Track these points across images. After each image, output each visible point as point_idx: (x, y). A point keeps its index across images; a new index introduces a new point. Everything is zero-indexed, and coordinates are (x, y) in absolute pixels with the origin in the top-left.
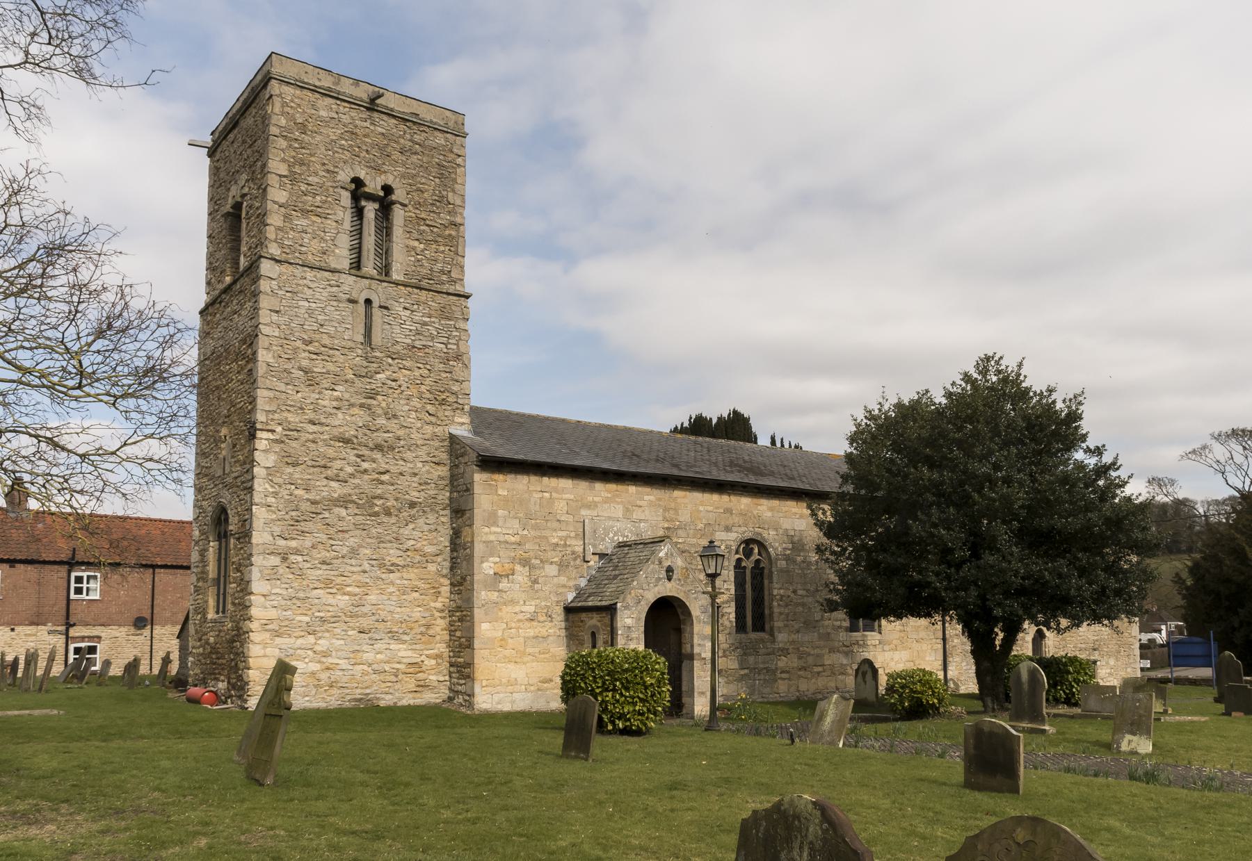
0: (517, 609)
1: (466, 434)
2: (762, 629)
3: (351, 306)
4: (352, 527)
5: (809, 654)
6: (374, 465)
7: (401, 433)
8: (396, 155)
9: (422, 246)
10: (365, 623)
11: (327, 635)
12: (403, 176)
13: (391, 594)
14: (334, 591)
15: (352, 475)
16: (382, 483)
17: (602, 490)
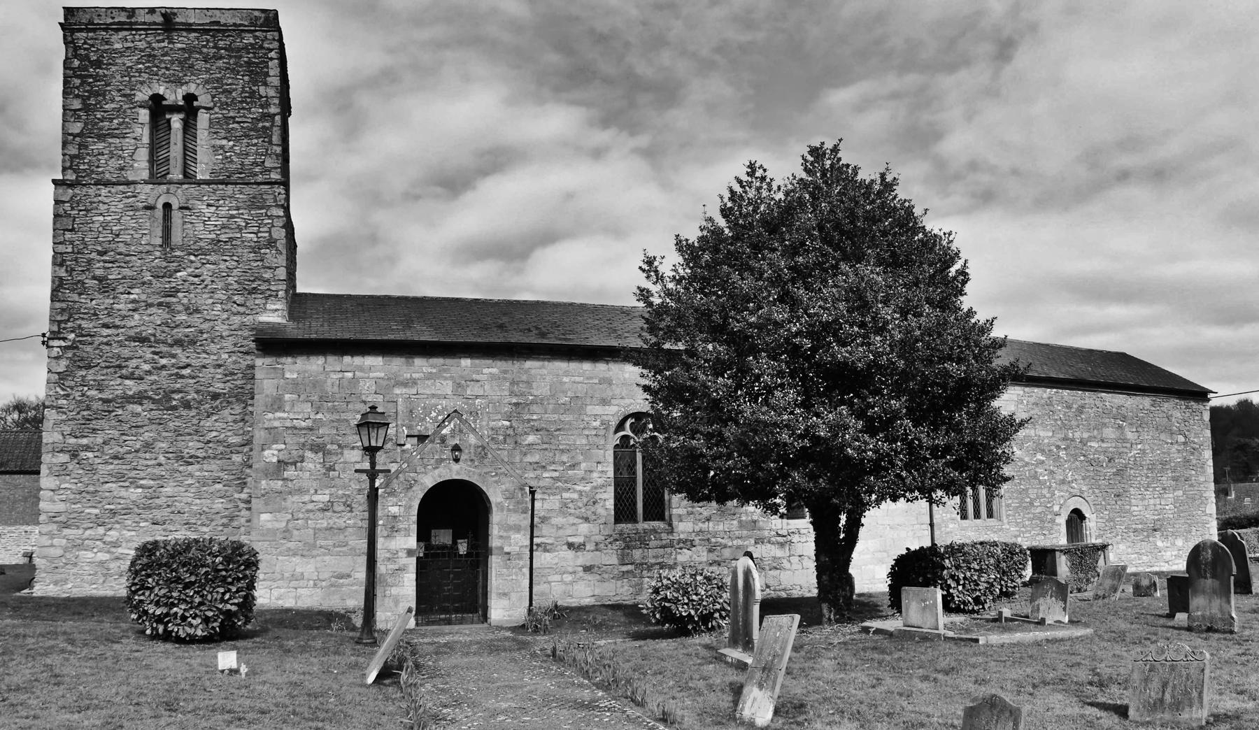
0: (306, 498)
1: (279, 320)
2: (661, 517)
3: (148, 212)
4: (147, 422)
5: (725, 546)
6: (173, 361)
7: (205, 326)
8: (200, 65)
9: (231, 143)
10: (158, 514)
11: (117, 526)
12: (207, 82)
13: (190, 485)
14: (127, 484)
15: (149, 373)
16: (182, 377)
17: (421, 365)
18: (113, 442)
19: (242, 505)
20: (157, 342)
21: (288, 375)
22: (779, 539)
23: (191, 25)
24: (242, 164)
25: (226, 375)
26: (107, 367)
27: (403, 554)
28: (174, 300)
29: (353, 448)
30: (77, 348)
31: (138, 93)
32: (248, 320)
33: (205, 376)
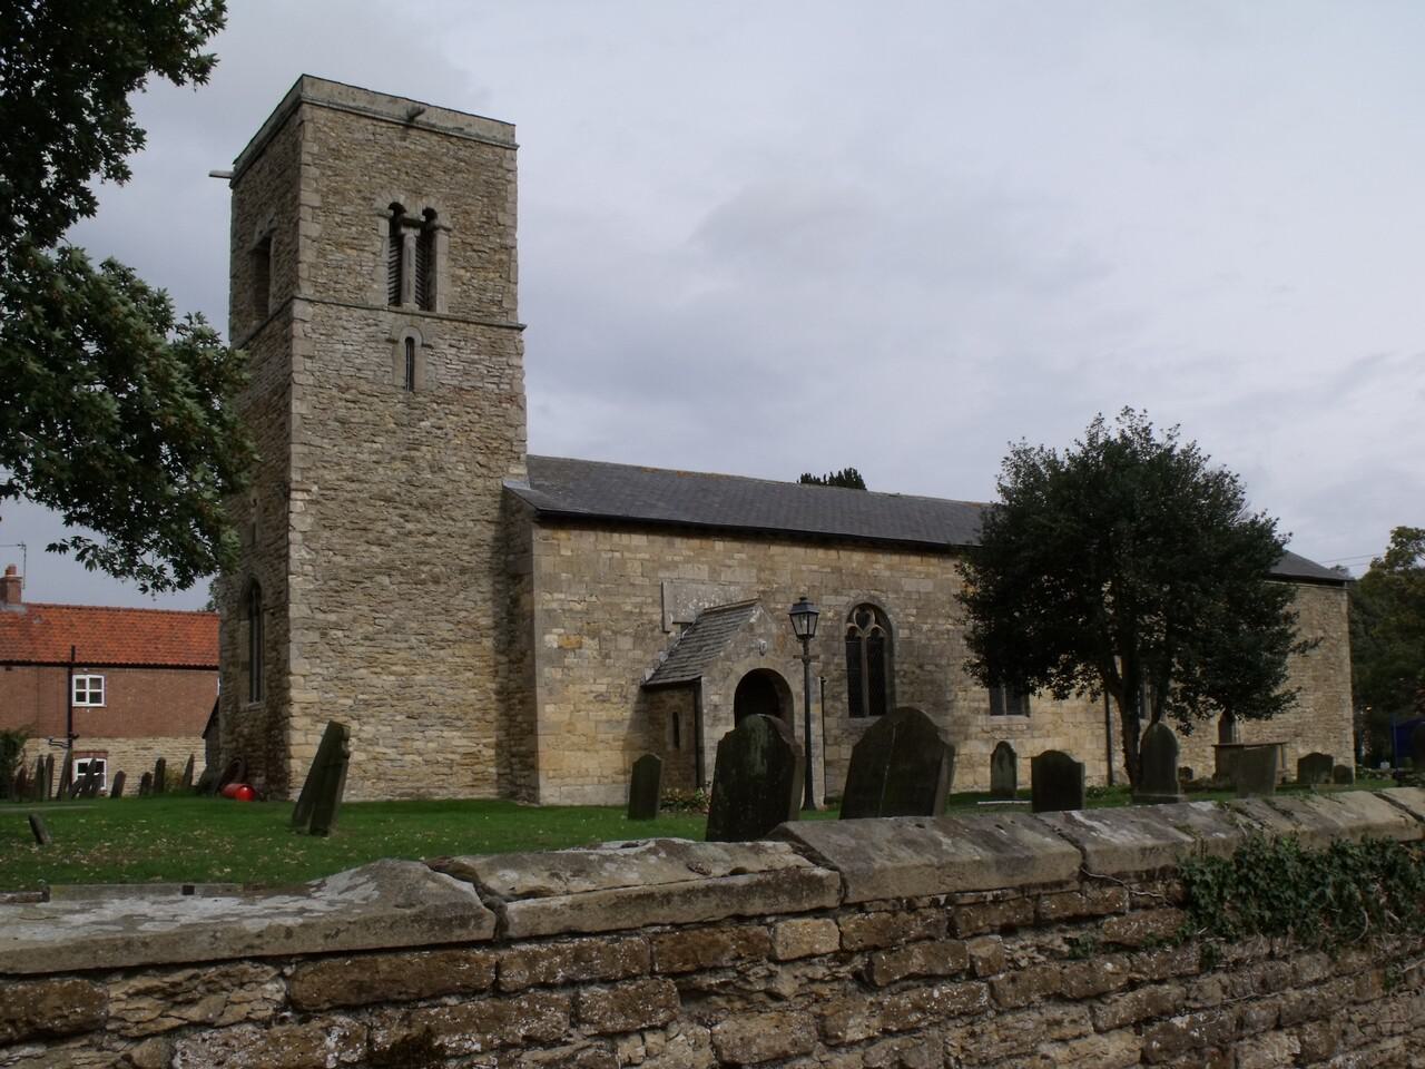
3: (390, 346)
6: (419, 526)
7: (448, 488)
8: (440, 176)
10: (415, 706)
11: (372, 720)
13: (441, 673)
15: (395, 539)
18: (362, 620)
21: (563, 552)
22: (986, 736)
23: (434, 126)
24: (480, 300)
28: (418, 454)
29: (626, 634)
31: (379, 199)
32: (491, 483)
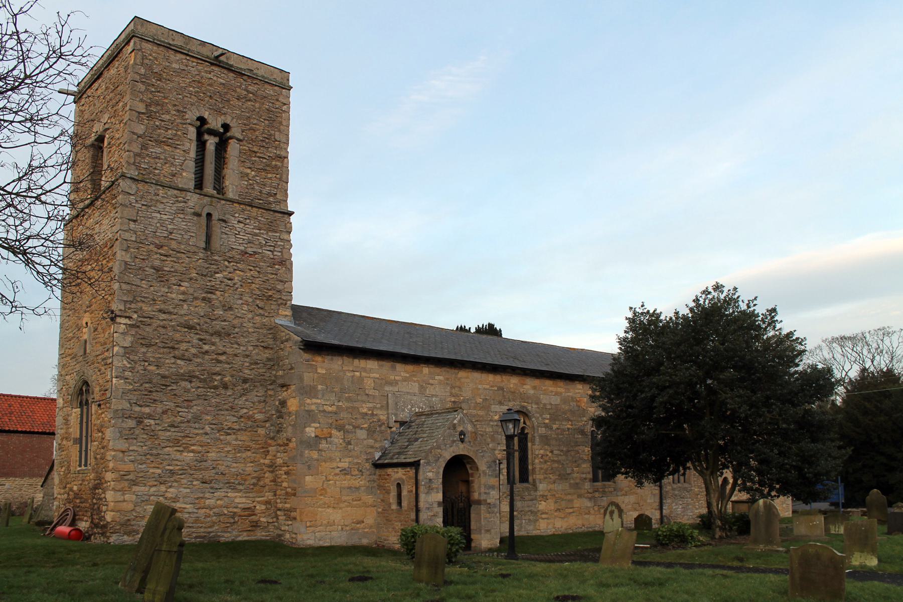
3: (195, 218)
6: (213, 348)
7: (236, 322)
10: (207, 475)
11: (175, 484)
15: (195, 355)
19: (266, 469)
20: (201, 330)
21: (319, 371)
25: (251, 364)
26: (164, 347)
27: (435, 505)
28: (214, 297)
29: (362, 428)
30: (138, 327)
31: (189, 112)
33: (238, 361)
